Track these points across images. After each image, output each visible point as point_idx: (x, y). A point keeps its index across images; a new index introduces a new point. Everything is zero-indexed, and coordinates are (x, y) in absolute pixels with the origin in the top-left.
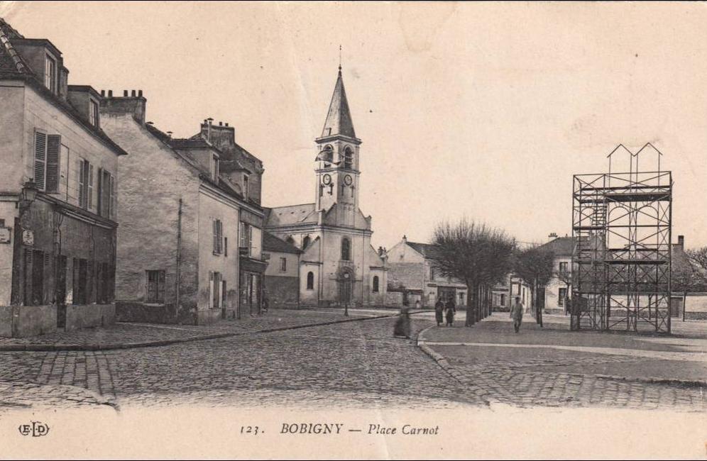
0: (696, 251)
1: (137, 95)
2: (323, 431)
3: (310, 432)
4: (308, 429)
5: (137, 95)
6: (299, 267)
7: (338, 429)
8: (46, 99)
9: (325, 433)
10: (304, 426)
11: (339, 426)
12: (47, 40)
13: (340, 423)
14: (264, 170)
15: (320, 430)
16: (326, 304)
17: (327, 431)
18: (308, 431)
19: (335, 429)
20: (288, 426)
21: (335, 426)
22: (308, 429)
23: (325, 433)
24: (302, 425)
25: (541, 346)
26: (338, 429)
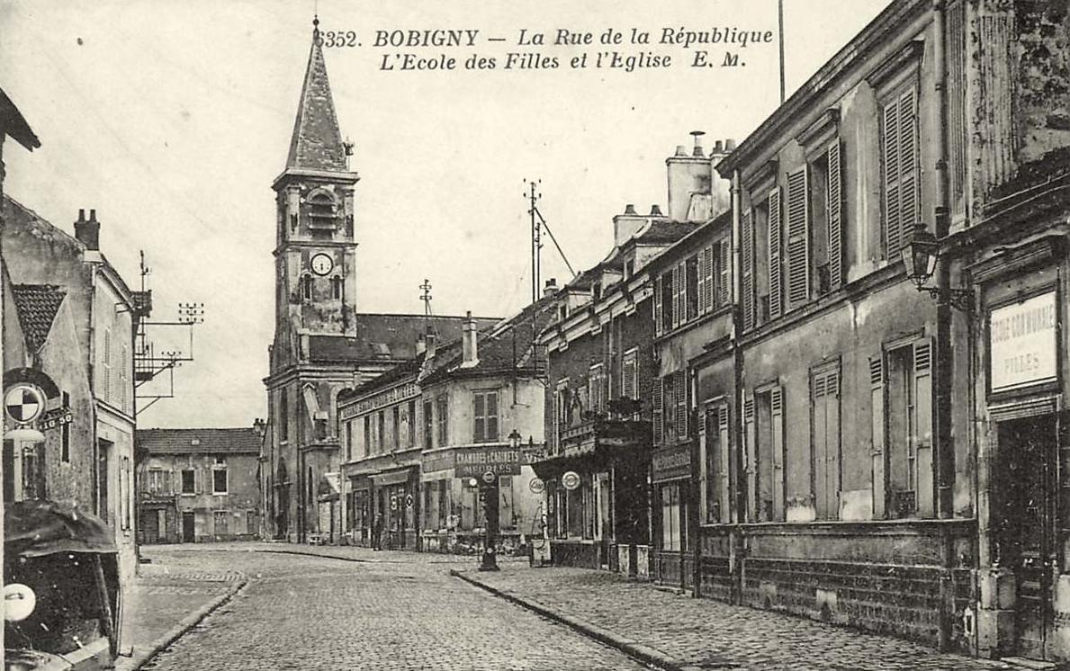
0: (927, 509)
1: (87, 218)
2: (446, 42)
3: (425, 44)
4: (422, 39)
5: (87, 218)
6: (1060, 373)
7: (472, 39)
8: (941, 41)
9: (449, 44)
10: (415, 35)
11: (473, 34)
12: (4, 175)
13: (472, 29)
14: (99, 224)
15: (442, 40)
16: (666, 484)
17: (453, 42)
18: (422, 42)
19: (465, 38)
20: (387, 35)
21: (465, 35)
22: (422, 39)
23: (449, 44)
24: (411, 32)
25: (610, 392)
26: (472, 39)
